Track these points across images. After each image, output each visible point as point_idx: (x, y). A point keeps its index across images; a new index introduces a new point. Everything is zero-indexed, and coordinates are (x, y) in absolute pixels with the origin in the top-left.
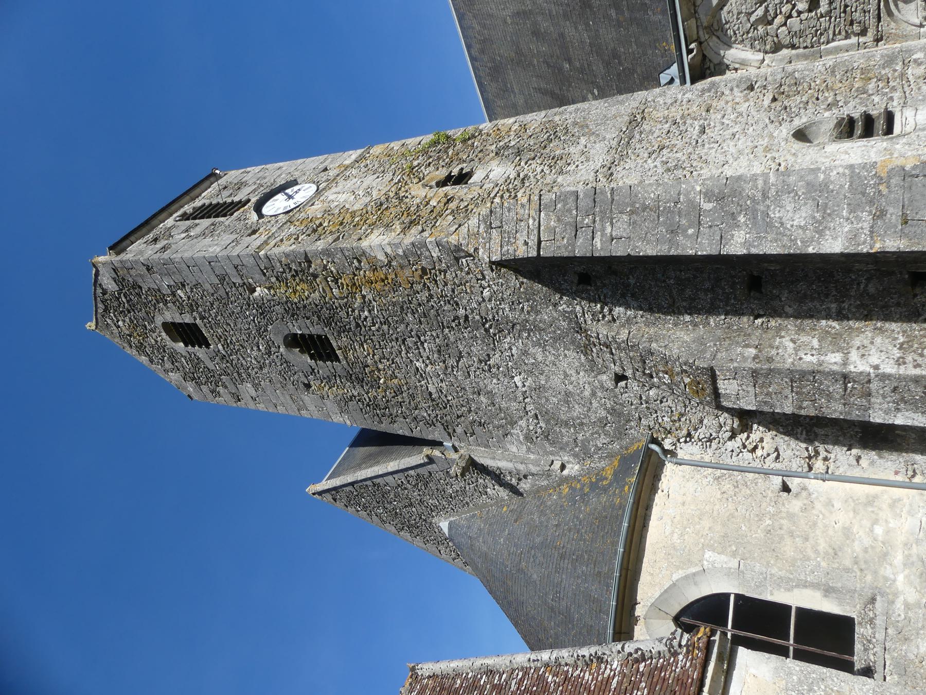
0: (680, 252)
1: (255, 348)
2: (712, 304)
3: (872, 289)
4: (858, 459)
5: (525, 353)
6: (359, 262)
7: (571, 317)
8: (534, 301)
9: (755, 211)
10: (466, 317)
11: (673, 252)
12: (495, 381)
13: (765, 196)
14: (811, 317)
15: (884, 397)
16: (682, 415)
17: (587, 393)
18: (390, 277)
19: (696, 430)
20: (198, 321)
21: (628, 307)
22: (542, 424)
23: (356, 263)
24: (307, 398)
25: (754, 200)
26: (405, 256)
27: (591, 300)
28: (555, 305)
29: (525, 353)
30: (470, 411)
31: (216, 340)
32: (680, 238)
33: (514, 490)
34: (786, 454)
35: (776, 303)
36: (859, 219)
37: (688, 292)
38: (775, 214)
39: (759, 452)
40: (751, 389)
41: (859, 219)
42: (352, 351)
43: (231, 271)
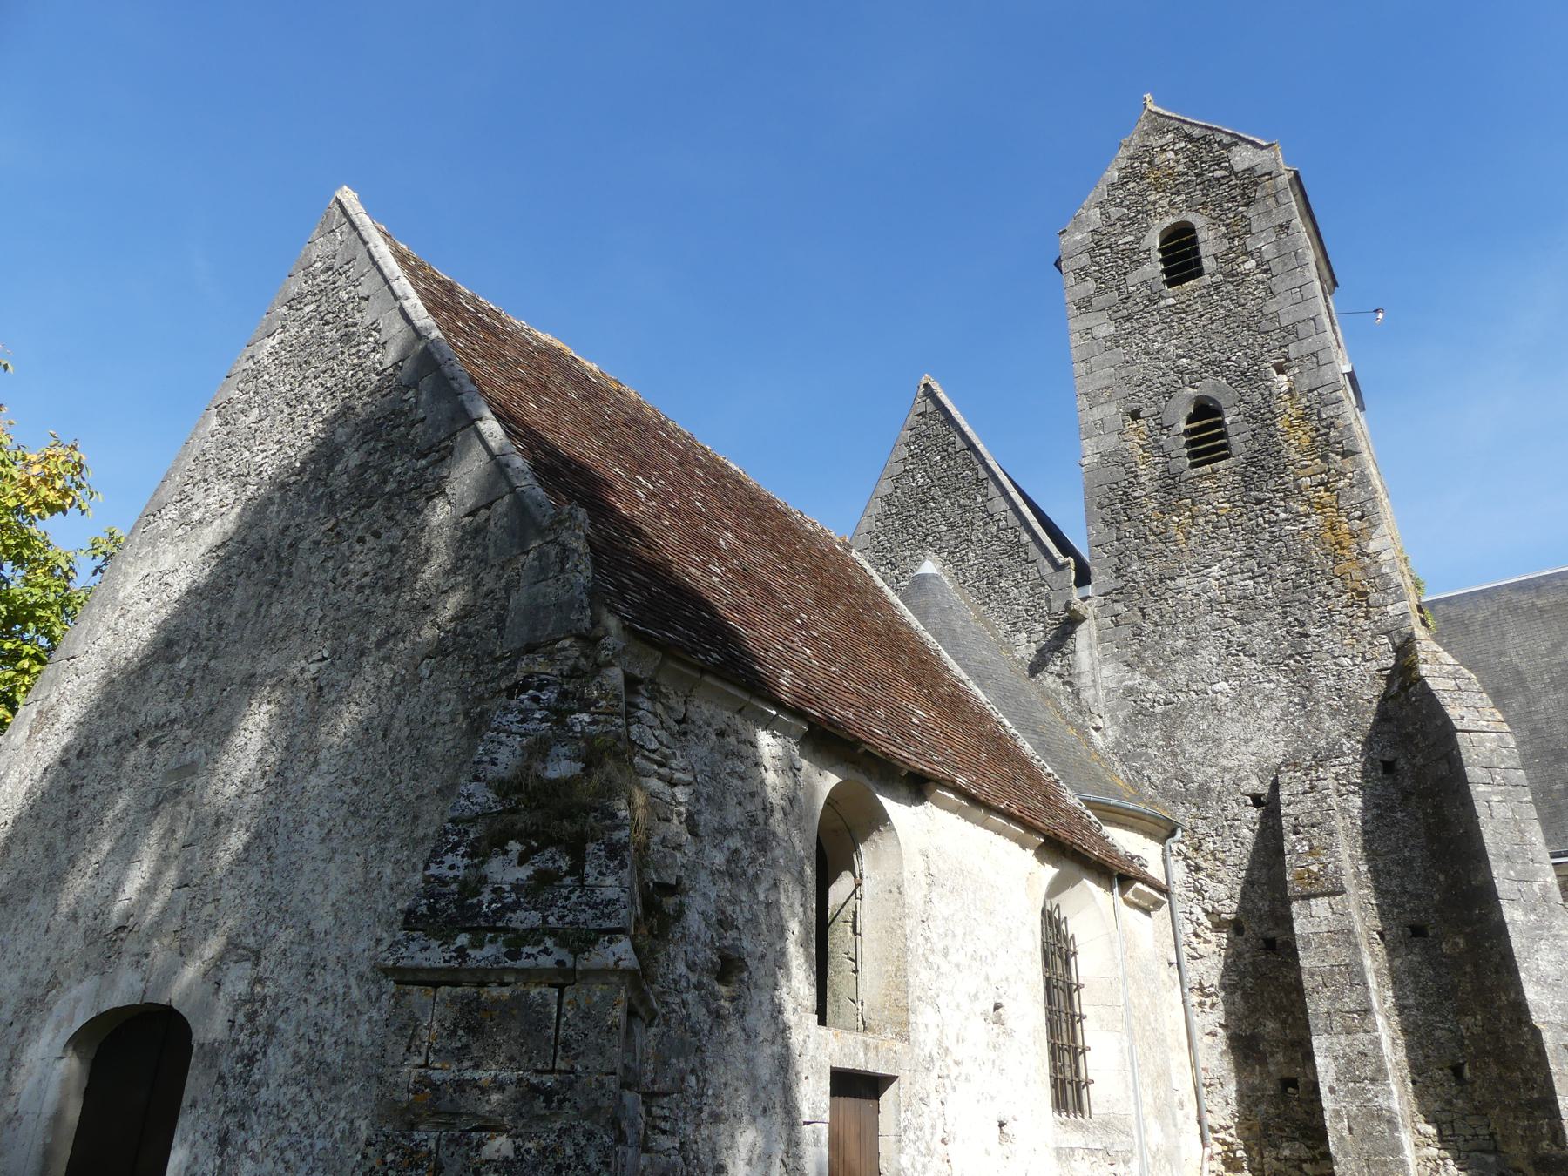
0: (1493, 864)
1: (1180, 351)
2: (1387, 892)
3: (1438, 1033)
4: (1214, 1034)
5: (1269, 698)
6: (1361, 518)
7: (1334, 751)
8: (1349, 714)
9: (1541, 928)
10: (1307, 636)
11: (1491, 858)
12: (1215, 659)
13: (1555, 936)
14: (1394, 983)
15: (1350, 1046)
16: (1223, 862)
17: (1224, 762)
18: (1345, 552)
19: (1209, 876)
20: (1207, 280)
21: (1365, 809)
22: (1158, 709)
23: (1358, 513)
24: (1112, 411)
25: (1550, 927)
26: (1382, 575)
27: (1364, 774)
28: (1348, 736)
29: (1269, 698)
30: (1156, 624)
31: (1182, 298)
32: (1504, 864)
33: (1036, 667)
34: (1201, 966)
35: (1403, 950)
36: (1555, 1012)
37: (1397, 869)
38: (1543, 945)
39: (1193, 939)
40: (1325, 928)
41: (1555, 1012)
42: (1217, 488)
43: (1306, 346)
